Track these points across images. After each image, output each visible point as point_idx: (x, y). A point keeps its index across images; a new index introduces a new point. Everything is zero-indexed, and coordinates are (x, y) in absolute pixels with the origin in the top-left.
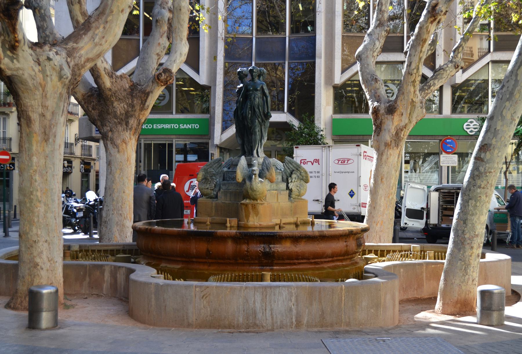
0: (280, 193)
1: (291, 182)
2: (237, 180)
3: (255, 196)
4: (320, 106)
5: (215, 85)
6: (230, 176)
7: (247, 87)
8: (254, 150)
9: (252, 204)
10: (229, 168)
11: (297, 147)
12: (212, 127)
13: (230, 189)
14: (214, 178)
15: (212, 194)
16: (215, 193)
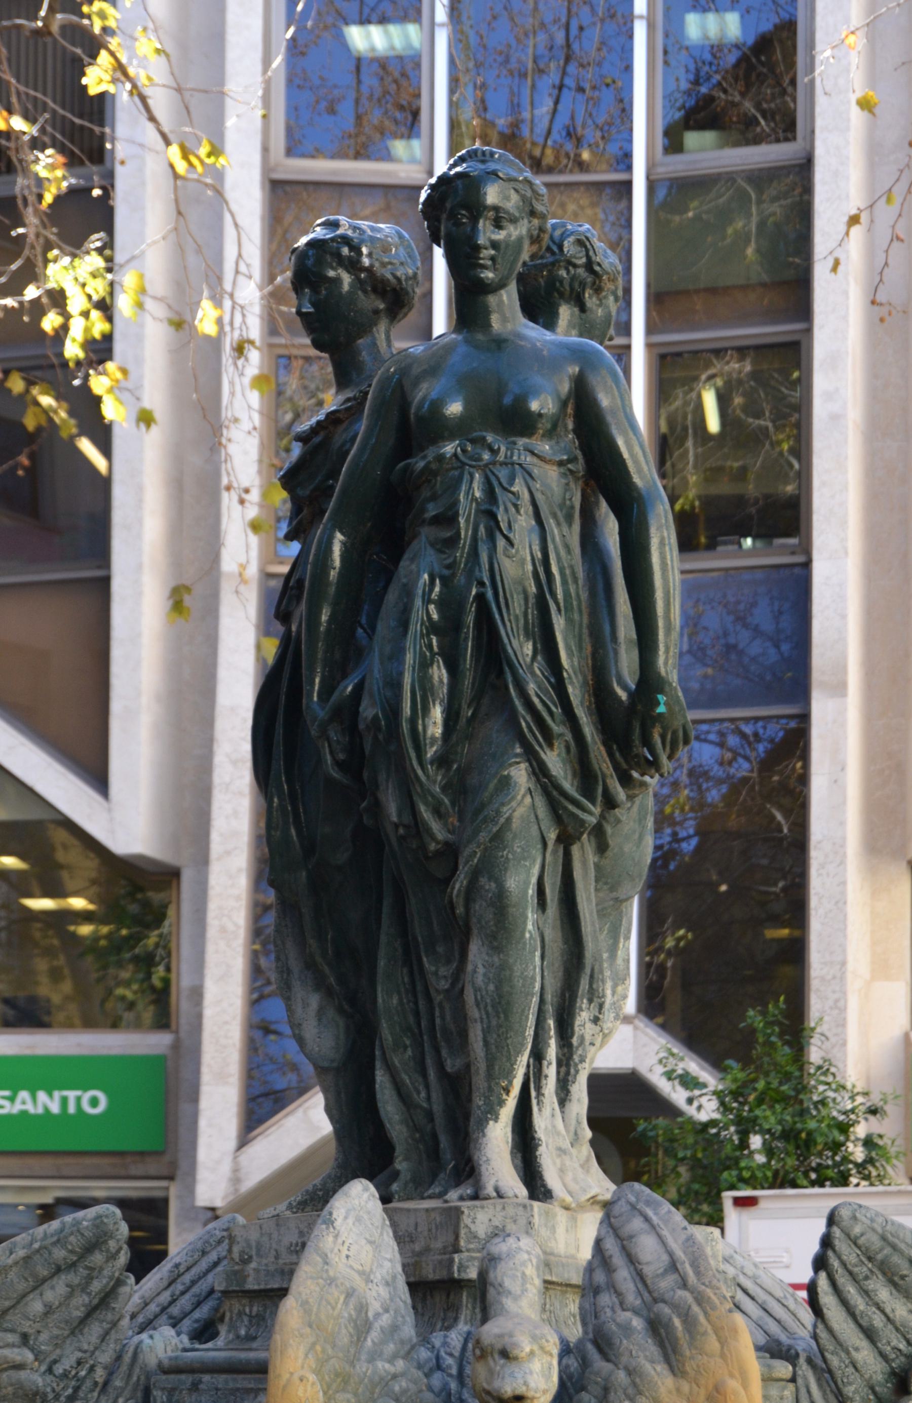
4: (841, 978)
5: (203, 860)
7: (404, 404)
8: (492, 1112)
12: (184, 1107)
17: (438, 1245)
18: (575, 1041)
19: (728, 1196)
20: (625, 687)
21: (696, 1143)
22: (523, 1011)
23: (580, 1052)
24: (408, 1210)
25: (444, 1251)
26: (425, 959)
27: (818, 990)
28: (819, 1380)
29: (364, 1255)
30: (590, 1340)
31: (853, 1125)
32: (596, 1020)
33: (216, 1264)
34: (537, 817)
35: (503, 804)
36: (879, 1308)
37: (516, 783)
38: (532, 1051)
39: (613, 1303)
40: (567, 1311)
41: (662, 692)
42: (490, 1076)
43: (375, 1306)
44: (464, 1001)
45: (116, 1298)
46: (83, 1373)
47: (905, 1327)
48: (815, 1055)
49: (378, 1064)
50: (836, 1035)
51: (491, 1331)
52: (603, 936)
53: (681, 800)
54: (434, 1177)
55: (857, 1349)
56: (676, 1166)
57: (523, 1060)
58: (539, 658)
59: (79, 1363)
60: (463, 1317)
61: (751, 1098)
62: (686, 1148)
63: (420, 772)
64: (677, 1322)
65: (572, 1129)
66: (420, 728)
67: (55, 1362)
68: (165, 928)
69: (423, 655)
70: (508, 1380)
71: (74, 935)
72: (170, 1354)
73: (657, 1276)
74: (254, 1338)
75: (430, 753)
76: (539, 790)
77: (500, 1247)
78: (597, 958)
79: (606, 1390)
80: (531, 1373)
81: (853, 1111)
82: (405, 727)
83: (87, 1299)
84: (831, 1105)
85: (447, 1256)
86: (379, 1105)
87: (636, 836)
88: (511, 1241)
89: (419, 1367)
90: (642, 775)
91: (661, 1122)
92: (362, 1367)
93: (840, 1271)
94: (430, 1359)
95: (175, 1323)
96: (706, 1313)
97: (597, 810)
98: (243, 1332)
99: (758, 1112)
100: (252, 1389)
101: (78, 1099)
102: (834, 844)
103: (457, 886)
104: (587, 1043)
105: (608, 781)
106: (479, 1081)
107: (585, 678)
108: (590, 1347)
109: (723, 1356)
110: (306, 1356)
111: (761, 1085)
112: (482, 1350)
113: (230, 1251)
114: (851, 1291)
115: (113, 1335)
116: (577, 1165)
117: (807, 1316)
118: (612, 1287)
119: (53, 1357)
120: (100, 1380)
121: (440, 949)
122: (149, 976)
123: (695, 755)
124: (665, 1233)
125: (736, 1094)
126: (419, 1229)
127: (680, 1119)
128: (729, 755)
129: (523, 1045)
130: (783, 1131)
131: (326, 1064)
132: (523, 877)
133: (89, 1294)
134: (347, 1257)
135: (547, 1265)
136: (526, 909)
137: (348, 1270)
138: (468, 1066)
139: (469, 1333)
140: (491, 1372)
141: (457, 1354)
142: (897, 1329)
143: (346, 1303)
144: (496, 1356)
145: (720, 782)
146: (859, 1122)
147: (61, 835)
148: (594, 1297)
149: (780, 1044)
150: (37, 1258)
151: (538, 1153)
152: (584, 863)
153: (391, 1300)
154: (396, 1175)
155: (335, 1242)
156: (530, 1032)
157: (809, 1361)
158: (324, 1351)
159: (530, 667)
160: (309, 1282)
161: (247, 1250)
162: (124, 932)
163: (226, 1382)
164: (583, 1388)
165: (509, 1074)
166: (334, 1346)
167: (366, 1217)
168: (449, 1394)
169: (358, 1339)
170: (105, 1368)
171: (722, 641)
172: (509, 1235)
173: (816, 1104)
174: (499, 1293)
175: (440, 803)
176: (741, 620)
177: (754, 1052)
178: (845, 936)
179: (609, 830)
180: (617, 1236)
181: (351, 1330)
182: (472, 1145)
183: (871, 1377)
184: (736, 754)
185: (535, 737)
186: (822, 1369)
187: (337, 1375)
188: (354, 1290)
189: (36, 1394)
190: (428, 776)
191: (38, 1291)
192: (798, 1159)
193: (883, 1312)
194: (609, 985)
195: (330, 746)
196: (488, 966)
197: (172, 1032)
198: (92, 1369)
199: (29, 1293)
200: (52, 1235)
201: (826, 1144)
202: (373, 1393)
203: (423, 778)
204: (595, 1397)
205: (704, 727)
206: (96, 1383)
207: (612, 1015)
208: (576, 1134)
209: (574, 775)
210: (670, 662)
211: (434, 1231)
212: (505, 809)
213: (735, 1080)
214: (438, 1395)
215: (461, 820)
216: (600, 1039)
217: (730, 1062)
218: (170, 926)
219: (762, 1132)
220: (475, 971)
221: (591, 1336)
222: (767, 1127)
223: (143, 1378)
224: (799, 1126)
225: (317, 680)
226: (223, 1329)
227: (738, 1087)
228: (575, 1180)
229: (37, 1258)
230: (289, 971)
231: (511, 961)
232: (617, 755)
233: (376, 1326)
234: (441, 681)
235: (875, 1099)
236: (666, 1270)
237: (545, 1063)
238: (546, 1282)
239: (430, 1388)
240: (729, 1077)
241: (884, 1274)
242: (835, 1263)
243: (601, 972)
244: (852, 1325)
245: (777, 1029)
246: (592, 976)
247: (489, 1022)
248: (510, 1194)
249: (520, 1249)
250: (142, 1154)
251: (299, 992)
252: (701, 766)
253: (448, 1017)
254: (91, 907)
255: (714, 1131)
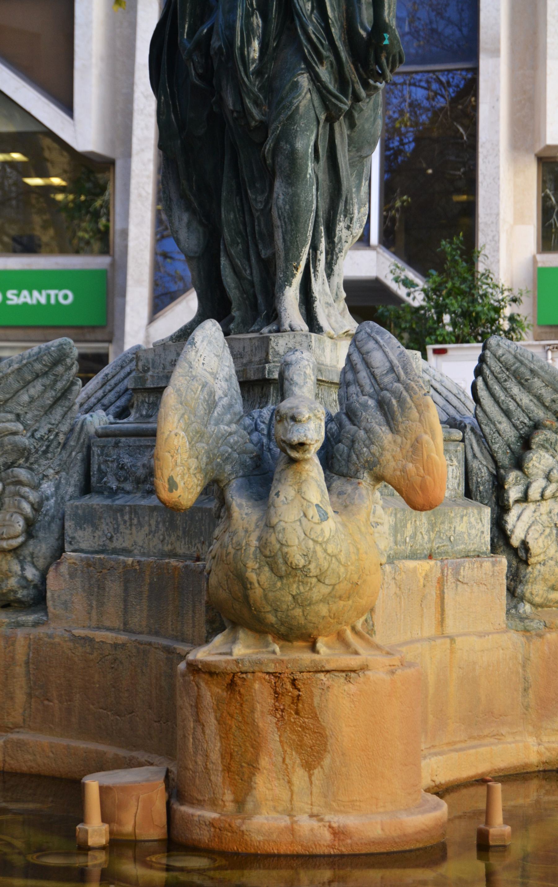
0: (456, 572)
1: (525, 498)
2: (164, 494)
3: (298, 612)
5: (128, 155)
6: (126, 460)
8: (288, 281)
9: (276, 675)
10: (122, 413)
11: (442, 352)
12: (118, 300)
13: (126, 551)
14: (23, 474)
15: (13, 582)
16: (31, 573)
17: (257, 359)
18: (336, 240)
19: (430, 348)
20: (365, 29)
21: (412, 319)
22: (306, 221)
23: (339, 246)
24: (240, 339)
25: (260, 362)
26: (249, 191)
27: (483, 230)
28: (478, 441)
29: (212, 363)
30: (344, 413)
31: (503, 308)
32: (348, 228)
33: (129, 374)
34: (314, 106)
35: (294, 98)
36: (513, 399)
37: (301, 86)
38: (311, 245)
39: (358, 392)
40: (331, 398)
41: (386, 32)
42: (287, 260)
43: (219, 393)
44: (271, 216)
45: (71, 393)
46: (52, 437)
47: (528, 410)
48: (481, 268)
49: (222, 254)
50: (494, 256)
51: (286, 405)
52: (353, 178)
53: (405, 119)
54: (254, 320)
55: (500, 423)
56: (400, 333)
57: (306, 251)
58: (315, 11)
59: (50, 431)
60: (271, 401)
61: (444, 292)
62: (406, 322)
63: (246, 79)
64: (394, 402)
65: (335, 292)
66: (246, 53)
67: (36, 430)
68: (106, 197)
69: (247, 9)
70: (295, 434)
71: (54, 200)
72: (102, 426)
73: (383, 375)
74: (151, 416)
75: (252, 68)
76: (315, 90)
77: (292, 358)
78: (349, 191)
79: (353, 442)
80: (309, 430)
81: (503, 300)
82: (237, 52)
83: (54, 393)
84: (490, 296)
85: (262, 366)
86: (223, 278)
87: (372, 119)
88: (298, 353)
89: (245, 429)
90: (375, 82)
91: (391, 307)
92: (212, 428)
93: (490, 376)
94: (251, 424)
95: (106, 408)
96: (411, 396)
97: (349, 103)
98: (144, 413)
99: (447, 301)
100: (149, 446)
101: (57, 296)
102: (492, 144)
103: (267, 147)
104: (343, 241)
105: (356, 85)
106: (281, 263)
107: (342, 23)
108: (344, 417)
109: (420, 421)
110: (179, 421)
111: (449, 285)
112: (281, 416)
113: (137, 365)
114: (496, 388)
115: (69, 415)
116: (337, 313)
117: (472, 405)
118: (357, 382)
119: (35, 428)
120: (62, 441)
121: (258, 185)
122: (97, 223)
123: (413, 95)
124: (387, 350)
125: (435, 291)
126: (246, 350)
127: (403, 305)
128: (431, 94)
129: (306, 241)
130: (462, 311)
131: (192, 255)
132: (306, 141)
133: (55, 390)
134: (203, 364)
135: (320, 370)
136: (307, 160)
137: (204, 372)
138: (274, 254)
139: (274, 410)
140: (286, 429)
141: (267, 422)
142: (523, 411)
143: (202, 390)
144: (289, 420)
145: (428, 110)
146: (506, 307)
147: (47, 142)
148: (347, 388)
149: (460, 260)
150: (25, 369)
151: (314, 305)
152: (342, 134)
153: (229, 390)
154: (232, 319)
155: (196, 355)
156: (310, 234)
157: (472, 430)
158: (189, 419)
159: (310, 18)
160: (181, 378)
161: (146, 364)
162: (83, 198)
163: (135, 441)
164: (340, 441)
165: (298, 258)
166: (195, 415)
167: (214, 341)
168: (262, 445)
169: (209, 412)
170: (65, 434)
171: (429, 27)
172: (297, 350)
173: (481, 296)
174: (291, 384)
175: (258, 97)
176: (440, 14)
177: (445, 266)
178: (499, 199)
179: (356, 115)
180: (360, 352)
181: (205, 407)
182: (276, 301)
183: (508, 439)
184: (436, 94)
185: (313, 58)
186: (480, 436)
187: (197, 432)
188: (207, 383)
189: (25, 449)
190: (250, 82)
191: (25, 389)
192: (471, 328)
193: (515, 400)
194: (356, 207)
195: (194, 65)
196: (286, 194)
197: (110, 255)
198: (57, 435)
199: (20, 390)
200: (33, 356)
201: (487, 319)
202: (218, 443)
203: (247, 83)
204: (347, 446)
205: (418, 77)
206: (59, 443)
207: (358, 225)
208: (337, 295)
209: (336, 81)
210: (391, 14)
211: (254, 351)
212: (295, 101)
213: (435, 282)
214: (256, 445)
215: (269, 108)
216: (351, 239)
217: (433, 272)
218: (109, 195)
219: (450, 313)
220: (278, 198)
221: (345, 411)
222: (452, 309)
223: (86, 440)
224: (471, 309)
225: (186, 26)
226: (133, 412)
227: (436, 286)
228: (336, 321)
229: (25, 369)
230: (171, 200)
231: (299, 191)
232: (361, 70)
233: (220, 404)
234: (258, 25)
235: (516, 293)
236: (387, 372)
237: (319, 252)
238: (318, 380)
239: (251, 441)
240: (431, 280)
241: (516, 378)
242: (487, 372)
243: (352, 199)
244: (497, 408)
245: (459, 252)
246: (346, 202)
247: (286, 228)
248: (298, 329)
249: (303, 358)
250: (93, 328)
251: (176, 212)
252: (416, 100)
253: (262, 226)
254: (63, 183)
255: (422, 312)
